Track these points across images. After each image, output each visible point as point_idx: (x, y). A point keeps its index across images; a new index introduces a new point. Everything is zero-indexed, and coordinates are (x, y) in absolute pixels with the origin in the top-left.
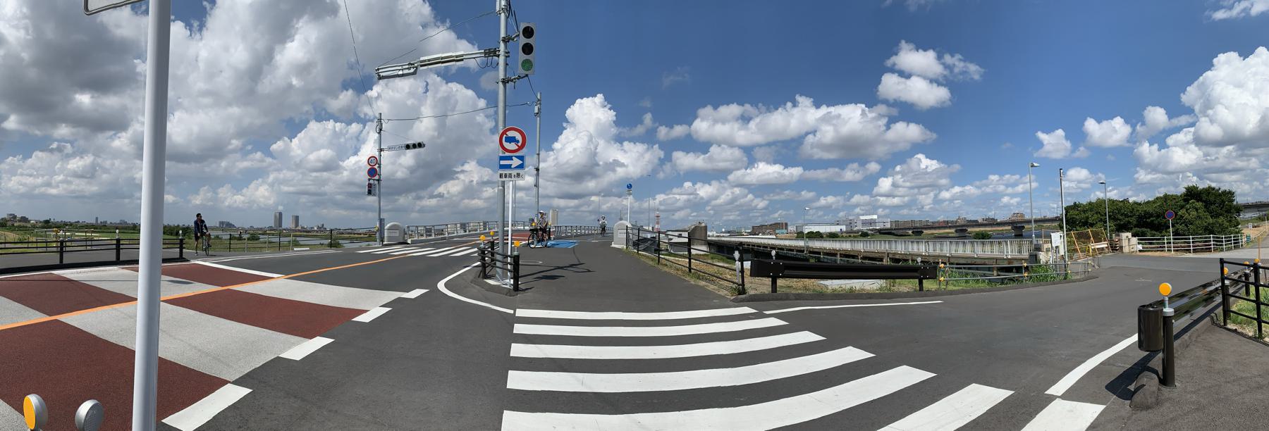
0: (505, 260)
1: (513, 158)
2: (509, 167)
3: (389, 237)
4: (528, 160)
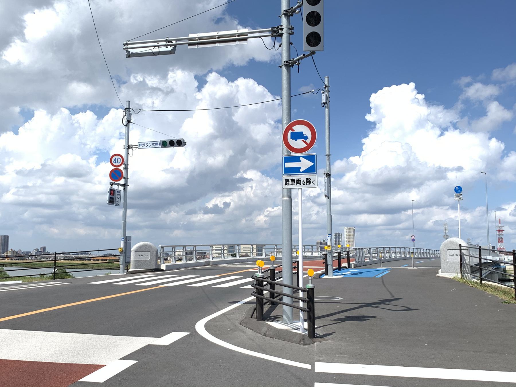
0: (295, 295)
1: (301, 159)
2: (297, 170)
3: (137, 262)
4: (319, 160)
